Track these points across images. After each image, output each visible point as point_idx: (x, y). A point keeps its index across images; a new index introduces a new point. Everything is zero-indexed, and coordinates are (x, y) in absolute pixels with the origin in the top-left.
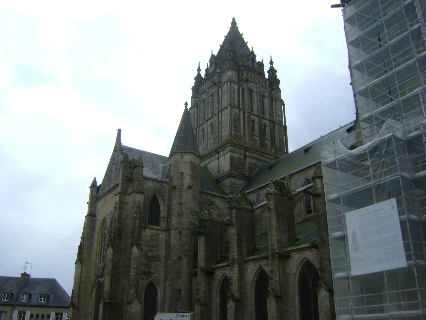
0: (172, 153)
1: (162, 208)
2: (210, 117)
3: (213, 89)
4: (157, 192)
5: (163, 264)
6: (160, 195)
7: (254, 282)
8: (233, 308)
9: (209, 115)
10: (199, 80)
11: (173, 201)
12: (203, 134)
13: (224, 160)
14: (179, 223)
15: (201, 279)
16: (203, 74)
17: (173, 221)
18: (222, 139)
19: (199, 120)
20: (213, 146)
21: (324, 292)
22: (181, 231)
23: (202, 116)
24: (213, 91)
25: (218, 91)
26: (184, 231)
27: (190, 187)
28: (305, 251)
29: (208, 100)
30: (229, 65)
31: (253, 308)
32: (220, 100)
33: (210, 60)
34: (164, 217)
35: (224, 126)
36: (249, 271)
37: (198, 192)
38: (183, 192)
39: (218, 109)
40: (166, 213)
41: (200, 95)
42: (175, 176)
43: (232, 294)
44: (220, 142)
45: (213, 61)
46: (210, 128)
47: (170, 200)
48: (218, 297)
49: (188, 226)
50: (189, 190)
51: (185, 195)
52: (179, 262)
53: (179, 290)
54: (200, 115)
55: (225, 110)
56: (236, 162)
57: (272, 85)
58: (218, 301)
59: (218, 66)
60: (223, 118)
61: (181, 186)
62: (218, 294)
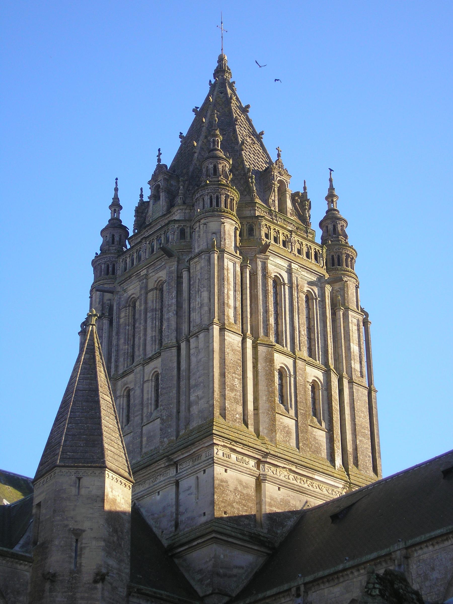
0: (47, 465)
2: (150, 354)
3: (161, 269)
9: (148, 348)
10: (117, 238)
12: (128, 405)
13: (193, 490)
16: (128, 219)
18: (188, 424)
19: (116, 361)
20: (161, 442)
23: (124, 347)
24: (163, 275)
25: (179, 277)
27: (100, 578)
29: (146, 303)
30: (214, 203)
32: (185, 306)
33: (154, 181)
35: (196, 385)
37: (123, 591)
38: (78, 595)
39: (178, 330)
41: (121, 283)
42: (57, 543)
44: (182, 433)
45: (162, 184)
46: (149, 387)
50: (99, 586)
54: (118, 345)
55: (201, 336)
56: (231, 497)
57: (333, 265)
59: (179, 200)
60: (193, 359)
61: (72, 572)
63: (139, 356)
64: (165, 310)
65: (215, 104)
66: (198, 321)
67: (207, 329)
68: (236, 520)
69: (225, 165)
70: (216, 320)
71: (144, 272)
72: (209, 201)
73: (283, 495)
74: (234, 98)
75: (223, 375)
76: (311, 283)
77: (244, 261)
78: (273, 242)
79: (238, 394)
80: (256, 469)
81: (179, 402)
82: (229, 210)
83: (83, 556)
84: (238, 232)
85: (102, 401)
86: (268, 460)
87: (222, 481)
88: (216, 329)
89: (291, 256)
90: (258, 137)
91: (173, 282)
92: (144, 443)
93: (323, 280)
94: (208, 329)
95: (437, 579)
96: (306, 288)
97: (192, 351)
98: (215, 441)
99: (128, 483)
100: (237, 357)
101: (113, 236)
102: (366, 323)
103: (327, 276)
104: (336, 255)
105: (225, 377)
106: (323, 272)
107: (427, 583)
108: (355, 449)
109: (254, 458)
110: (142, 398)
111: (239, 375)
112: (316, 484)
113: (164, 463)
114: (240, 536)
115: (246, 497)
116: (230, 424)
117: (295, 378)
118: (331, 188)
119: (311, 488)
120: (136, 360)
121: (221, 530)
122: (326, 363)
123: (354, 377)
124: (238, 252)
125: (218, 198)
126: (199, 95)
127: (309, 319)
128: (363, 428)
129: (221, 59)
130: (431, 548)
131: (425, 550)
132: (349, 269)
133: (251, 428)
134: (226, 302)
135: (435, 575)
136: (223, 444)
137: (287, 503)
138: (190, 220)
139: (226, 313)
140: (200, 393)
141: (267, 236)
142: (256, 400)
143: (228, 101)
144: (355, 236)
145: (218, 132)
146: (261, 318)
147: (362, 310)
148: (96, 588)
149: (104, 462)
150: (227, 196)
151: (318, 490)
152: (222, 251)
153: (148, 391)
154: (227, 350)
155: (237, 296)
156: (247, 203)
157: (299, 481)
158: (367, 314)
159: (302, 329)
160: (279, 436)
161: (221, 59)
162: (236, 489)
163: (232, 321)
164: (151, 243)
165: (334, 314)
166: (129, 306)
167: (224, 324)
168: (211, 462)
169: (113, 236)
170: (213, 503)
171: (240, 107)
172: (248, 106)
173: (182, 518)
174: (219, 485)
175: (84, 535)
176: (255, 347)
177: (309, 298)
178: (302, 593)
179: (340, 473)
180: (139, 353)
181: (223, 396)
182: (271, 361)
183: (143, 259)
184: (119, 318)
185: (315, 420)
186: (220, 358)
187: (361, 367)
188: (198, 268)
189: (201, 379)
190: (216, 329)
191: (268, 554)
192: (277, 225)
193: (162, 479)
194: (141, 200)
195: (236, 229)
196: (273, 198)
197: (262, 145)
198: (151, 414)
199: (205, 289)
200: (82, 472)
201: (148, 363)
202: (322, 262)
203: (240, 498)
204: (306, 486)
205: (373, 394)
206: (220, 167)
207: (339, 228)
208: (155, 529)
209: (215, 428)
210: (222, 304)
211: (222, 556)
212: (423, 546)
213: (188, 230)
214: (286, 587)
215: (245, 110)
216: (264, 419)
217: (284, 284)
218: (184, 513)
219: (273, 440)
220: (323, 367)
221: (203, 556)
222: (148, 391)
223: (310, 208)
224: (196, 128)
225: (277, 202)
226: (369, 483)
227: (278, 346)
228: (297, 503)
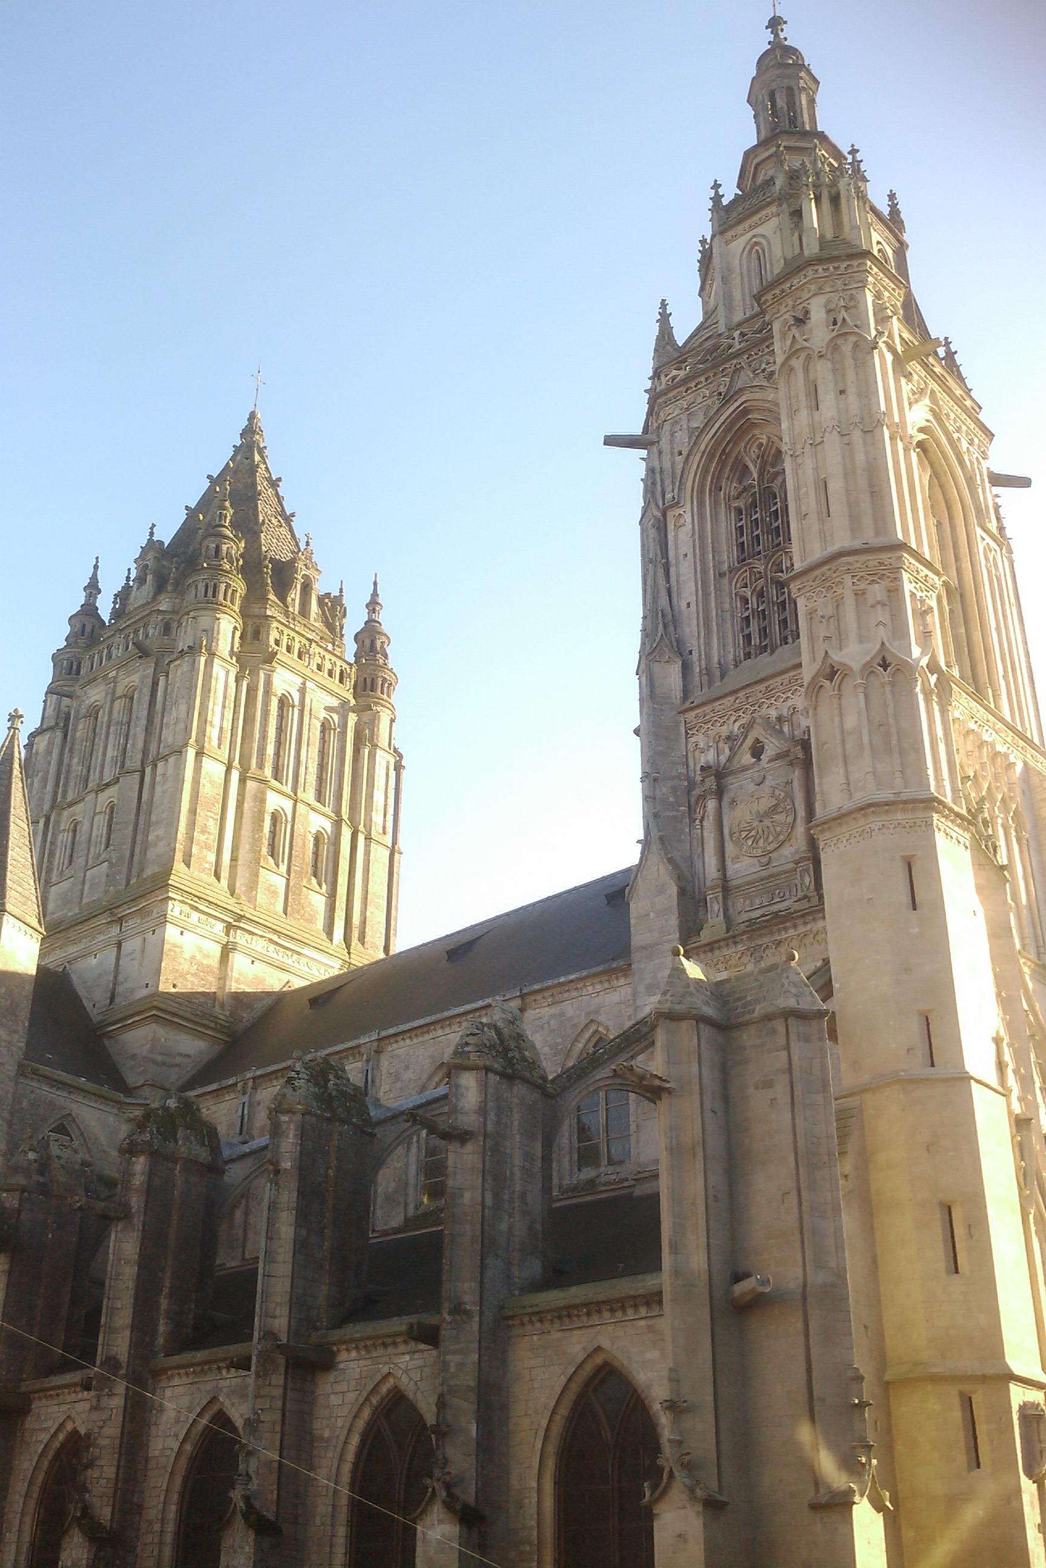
2: (107, 779)
7: (183, 1461)
10: (88, 629)
12: (73, 843)
16: (105, 608)
19: (66, 785)
20: (106, 892)
21: (440, 1522)
23: (77, 768)
25: (155, 684)
28: (390, 1350)
29: (111, 713)
30: (210, 593)
32: (157, 720)
35: (158, 823)
39: (145, 751)
43: (85, 1509)
46: (101, 821)
48: (28, 1519)
54: (69, 765)
55: (172, 760)
56: (185, 967)
58: (27, 1538)
60: (158, 789)
62: (32, 1505)
63: (93, 780)
64: (132, 724)
65: (236, 472)
66: (170, 740)
67: (180, 752)
68: (189, 998)
69: (233, 547)
70: (192, 741)
71: (113, 674)
72: (203, 590)
73: (259, 971)
74: (263, 466)
75: (193, 812)
76: (328, 709)
77: (242, 668)
78: (284, 650)
79: (212, 837)
80: (223, 935)
81: (134, 842)
82: (229, 603)
84: (238, 634)
85: (12, 826)
86: (241, 925)
87: (175, 946)
88: (191, 753)
89: (308, 672)
90: (288, 519)
92: (86, 892)
93: (347, 707)
95: (410, 1080)
97: (158, 779)
98: (170, 894)
99: (35, 935)
100: (216, 791)
101: (84, 625)
102: (398, 767)
103: (353, 702)
104: (369, 679)
107: (398, 1085)
108: (364, 922)
109: (224, 921)
110: (91, 835)
111: (216, 814)
112: (303, 960)
114: (193, 1018)
115: (207, 969)
116: (196, 873)
117: (293, 826)
118: (375, 594)
119: (296, 965)
120: (90, 785)
121: (164, 1007)
122: (338, 812)
123: (373, 833)
124: (234, 658)
125: (215, 587)
126: (218, 459)
127: (323, 753)
128: (378, 897)
129: (252, 416)
130: (408, 1042)
131: (401, 1043)
132: (385, 697)
133: (224, 883)
134: (209, 719)
135: (408, 1075)
136: (181, 898)
137: (262, 981)
138: (177, 613)
139: (207, 734)
140: (160, 832)
141: (277, 642)
142: (235, 849)
143: (253, 469)
144: (398, 657)
145: (227, 504)
147: (395, 750)
149: (3, 904)
150: (228, 586)
151: (306, 969)
154: (202, 781)
156: (255, 596)
157: (281, 955)
158: (401, 756)
159: (310, 765)
160: (261, 898)
161: (252, 416)
162: (193, 958)
163: (215, 743)
164: (127, 637)
165: (357, 751)
167: (203, 747)
168: (163, 920)
169: (84, 625)
170: (158, 972)
171: (269, 479)
172: (279, 479)
173: (120, 989)
174: (170, 950)
176: (243, 780)
177: (325, 727)
178: (249, 1090)
179: (338, 950)
180: (94, 777)
181: (190, 839)
182: (261, 800)
183: (114, 657)
184: (75, 730)
185: (314, 880)
187: (385, 821)
188: (179, 673)
189: (164, 815)
190: (191, 753)
191: (226, 1042)
192: (294, 630)
193: (102, 938)
194: (127, 584)
195: (235, 628)
196: (293, 596)
197: (291, 530)
198: (99, 855)
201: (102, 790)
202: (349, 683)
204: (290, 962)
205: (397, 856)
206: (224, 547)
207: (378, 645)
208: (86, 1003)
209: (172, 877)
210: (204, 721)
211: (163, 1040)
212: (399, 1038)
213: (175, 625)
214: (231, 1081)
215: (274, 484)
216: (242, 873)
217: (293, 706)
219: (252, 900)
220: (333, 815)
221: (139, 1039)
223: (344, 615)
224: (206, 501)
225: (297, 602)
226: (367, 962)
227: (274, 783)
228: (274, 982)
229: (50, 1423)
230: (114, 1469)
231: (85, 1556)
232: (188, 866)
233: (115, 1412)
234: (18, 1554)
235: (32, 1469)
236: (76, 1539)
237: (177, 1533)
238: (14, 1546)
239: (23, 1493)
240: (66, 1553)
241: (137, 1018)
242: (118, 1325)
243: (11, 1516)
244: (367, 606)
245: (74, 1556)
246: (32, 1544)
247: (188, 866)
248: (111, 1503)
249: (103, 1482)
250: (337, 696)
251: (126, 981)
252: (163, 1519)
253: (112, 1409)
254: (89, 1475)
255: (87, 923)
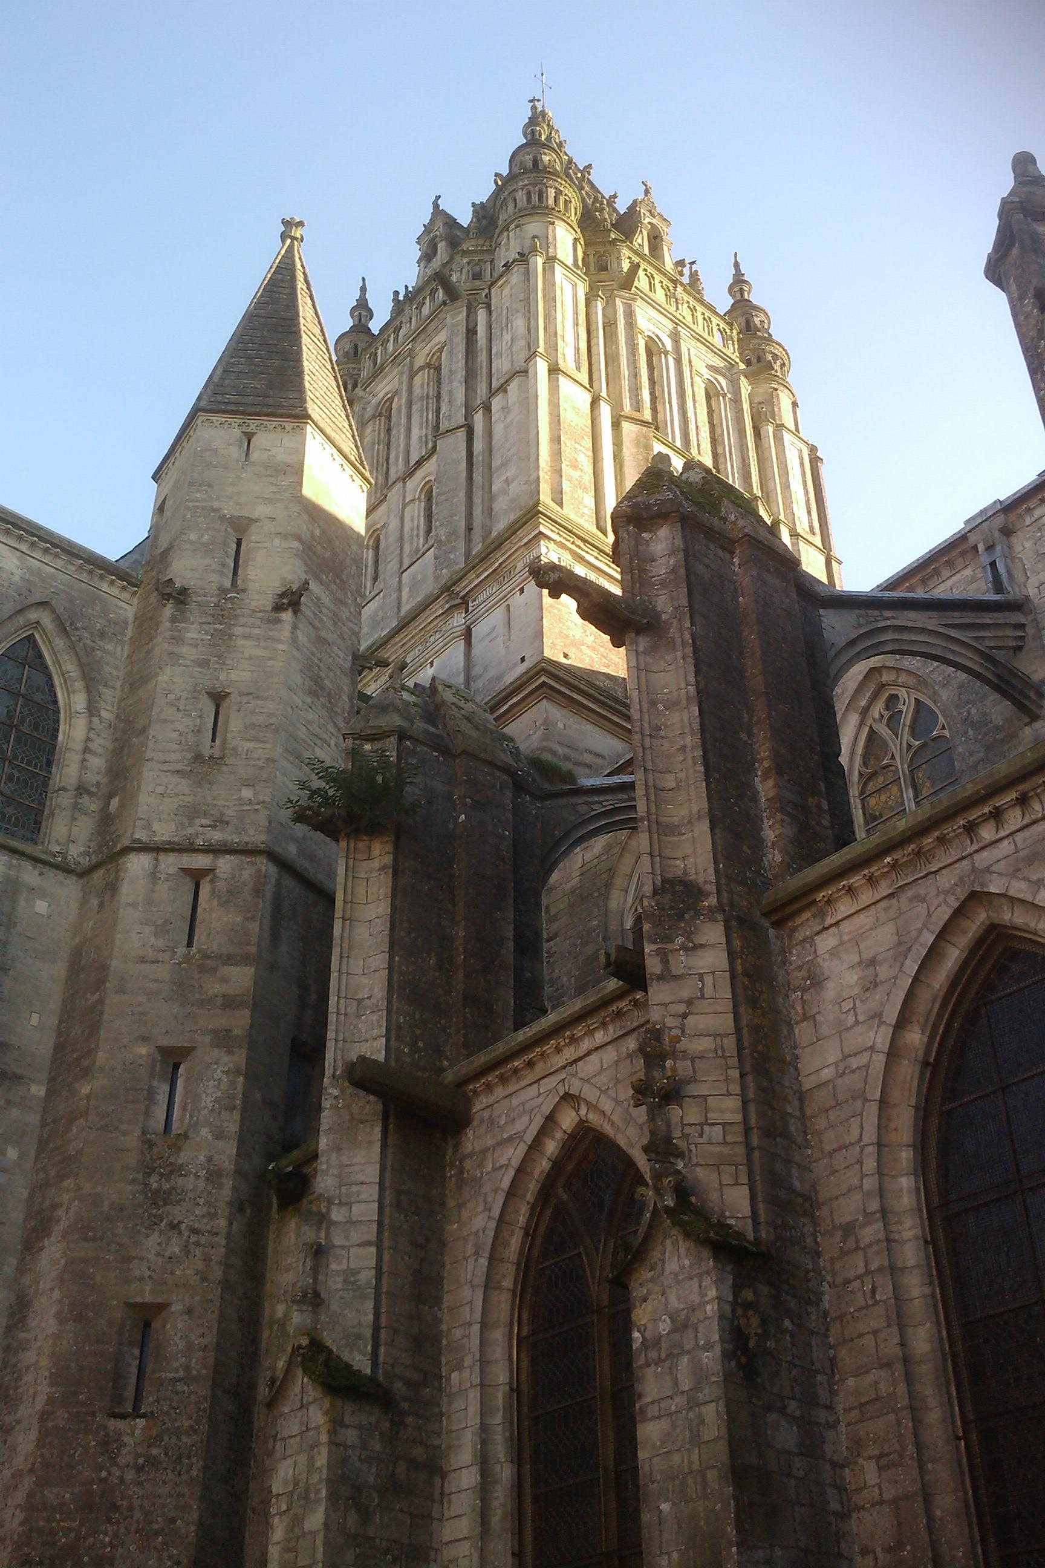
1: (73, 731)
4: (46, 619)
5: (34, 1119)
6: (73, 647)
7: (908, 1072)
8: (712, 1332)
11: (163, 678)
14: (192, 812)
15: (352, 1166)
17: (144, 799)
20: (437, 578)
22: (201, 861)
26: (225, 864)
27: (290, 600)
31: (923, 1339)
34: (81, 789)
35: (504, 464)
36: (841, 976)
38: (238, 631)
40: (97, 763)
43: (683, 1191)
47: (138, 680)
48: (498, 1335)
49: (263, 838)
50: (287, 616)
51: (248, 648)
52: (162, 1090)
53: (145, 1319)
55: (513, 387)
58: (501, 1375)
61: (223, 591)
62: (503, 1304)
67: (524, 372)
75: (556, 440)
83: (250, 563)
85: (305, 339)
88: (542, 366)
91: (460, 337)
94: (526, 372)
96: (707, 374)
98: (542, 529)
102: (815, 460)
105: (559, 443)
106: (736, 356)
113: (442, 607)
146: (625, 384)
148: (278, 621)
150: (558, 193)
152: (551, 260)
153: (413, 517)
155: (580, 333)
165: (757, 434)
166: (380, 415)
169: (356, 347)
170: (539, 634)
175: (254, 528)
176: (616, 425)
181: (558, 472)
186: (551, 414)
196: (639, 241)
199: (520, 315)
200: (253, 424)
203: (594, 641)
205: (834, 565)
211: (560, 725)
218: (481, 675)
222: (413, 517)
229: (520, 1125)
230: (734, 1103)
231: (713, 1293)
232: (561, 505)
233: (708, 980)
234: (485, 1411)
235: (493, 1225)
236: (672, 1265)
237: (930, 1241)
238: (474, 1395)
239: (480, 1279)
240: (649, 1306)
241: (515, 700)
242: (675, 820)
243: (458, 1333)
244: (730, 289)
245: (674, 1303)
246: (515, 1390)
247: (561, 505)
248: (744, 1179)
249: (717, 1132)
250: (723, 357)
251: (485, 669)
252: (884, 1212)
253: (701, 977)
254: (675, 1120)
255: (413, 625)
